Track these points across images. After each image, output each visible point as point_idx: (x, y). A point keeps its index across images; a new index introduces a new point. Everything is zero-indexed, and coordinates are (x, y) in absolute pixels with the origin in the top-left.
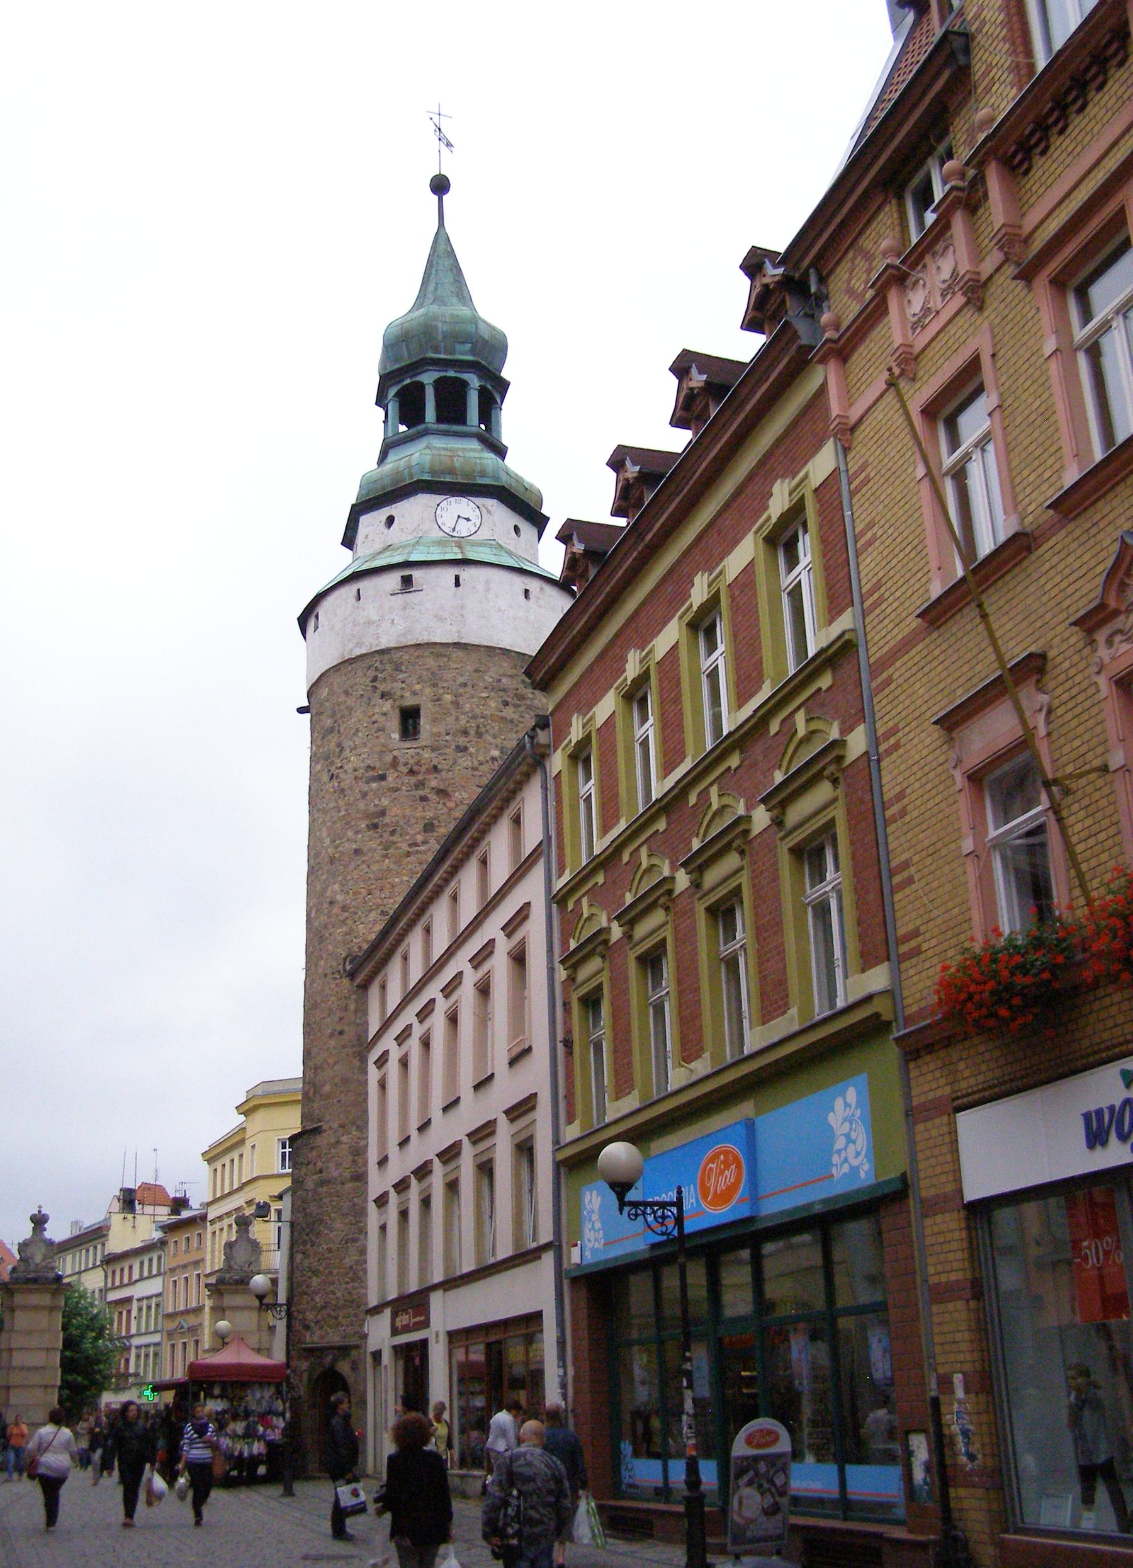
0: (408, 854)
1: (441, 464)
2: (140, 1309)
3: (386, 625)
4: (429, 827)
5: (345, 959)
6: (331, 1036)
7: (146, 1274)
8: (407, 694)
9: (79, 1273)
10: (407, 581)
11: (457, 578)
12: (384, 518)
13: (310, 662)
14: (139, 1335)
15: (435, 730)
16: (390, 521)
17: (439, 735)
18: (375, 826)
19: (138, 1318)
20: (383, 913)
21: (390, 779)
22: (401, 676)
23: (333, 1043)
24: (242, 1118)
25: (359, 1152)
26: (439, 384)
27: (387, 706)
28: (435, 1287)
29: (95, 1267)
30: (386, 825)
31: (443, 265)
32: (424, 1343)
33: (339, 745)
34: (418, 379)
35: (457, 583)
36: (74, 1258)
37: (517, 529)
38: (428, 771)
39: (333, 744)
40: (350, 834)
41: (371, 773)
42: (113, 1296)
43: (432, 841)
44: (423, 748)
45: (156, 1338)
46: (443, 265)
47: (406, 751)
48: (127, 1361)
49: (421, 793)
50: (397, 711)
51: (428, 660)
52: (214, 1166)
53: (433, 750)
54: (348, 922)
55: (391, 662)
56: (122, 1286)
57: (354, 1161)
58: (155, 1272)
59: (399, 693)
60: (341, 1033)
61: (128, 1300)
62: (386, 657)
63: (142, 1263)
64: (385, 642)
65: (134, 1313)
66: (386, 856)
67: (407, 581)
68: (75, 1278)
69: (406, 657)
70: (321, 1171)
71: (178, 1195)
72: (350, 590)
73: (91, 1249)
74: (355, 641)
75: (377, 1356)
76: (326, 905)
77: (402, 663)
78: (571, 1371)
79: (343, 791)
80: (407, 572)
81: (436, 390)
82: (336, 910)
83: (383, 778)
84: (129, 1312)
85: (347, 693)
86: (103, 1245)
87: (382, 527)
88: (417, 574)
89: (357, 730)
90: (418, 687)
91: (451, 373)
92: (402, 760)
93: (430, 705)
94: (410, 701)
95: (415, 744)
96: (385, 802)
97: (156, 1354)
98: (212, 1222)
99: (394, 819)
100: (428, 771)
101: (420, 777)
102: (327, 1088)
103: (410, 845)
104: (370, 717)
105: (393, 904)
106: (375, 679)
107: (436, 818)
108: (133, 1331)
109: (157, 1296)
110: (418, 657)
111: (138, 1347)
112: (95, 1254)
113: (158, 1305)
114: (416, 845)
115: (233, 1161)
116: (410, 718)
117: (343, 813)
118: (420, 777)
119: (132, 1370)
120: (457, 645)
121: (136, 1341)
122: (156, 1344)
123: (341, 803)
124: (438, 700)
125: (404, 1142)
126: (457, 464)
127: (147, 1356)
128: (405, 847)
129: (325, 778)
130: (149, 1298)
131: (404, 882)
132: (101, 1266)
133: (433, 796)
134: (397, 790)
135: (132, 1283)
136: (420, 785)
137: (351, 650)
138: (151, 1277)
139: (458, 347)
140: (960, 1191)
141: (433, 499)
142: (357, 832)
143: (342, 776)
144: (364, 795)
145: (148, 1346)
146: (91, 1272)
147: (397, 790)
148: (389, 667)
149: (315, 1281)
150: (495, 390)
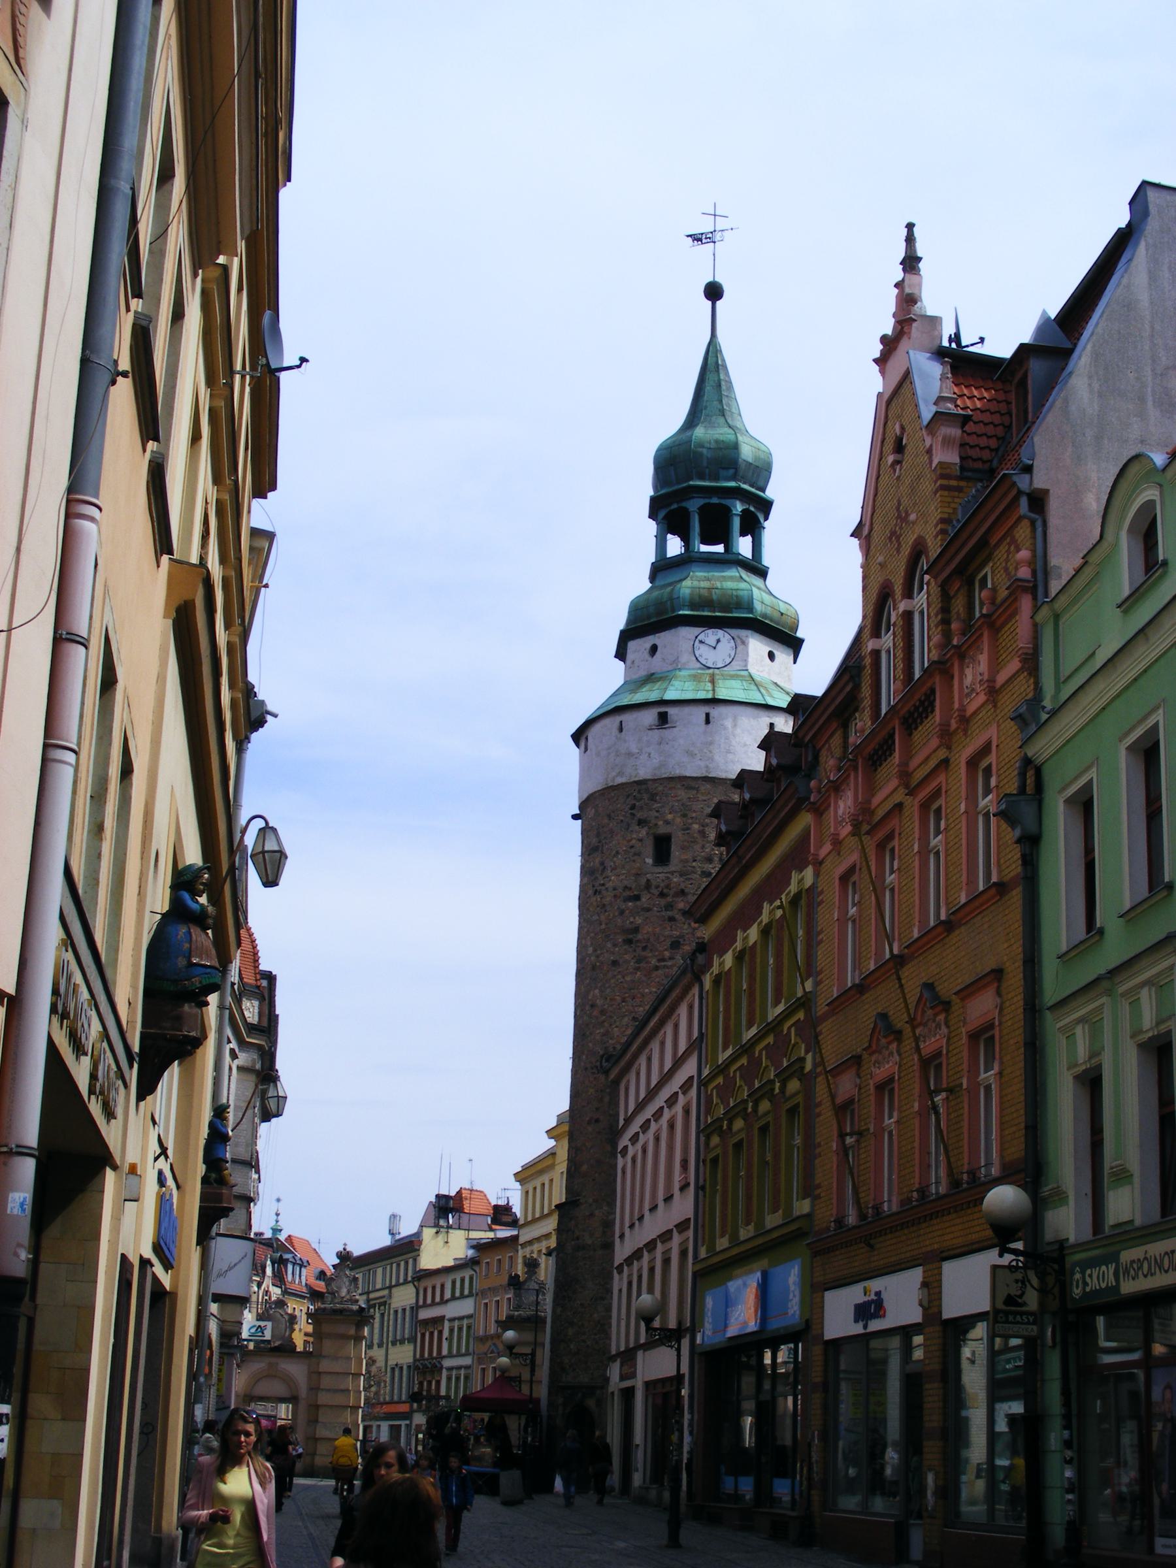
0: (657, 968)
1: (700, 596)
2: (451, 1330)
3: (644, 757)
4: (675, 945)
5: (602, 1056)
6: (589, 1123)
7: (458, 1294)
8: (661, 823)
9: (390, 1287)
10: (663, 719)
11: (707, 715)
12: (648, 645)
13: (585, 772)
14: (450, 1355)
15: (684, 857)
16: (654, 649)
17: (687, 861)
18: (629, 942)
19: (450, 1339)
20: (634, 1019)
21: (644, 900)
22: (656, 805)
23: (590, 1129)
24: (552, 1143)
25: (608, 1225)
26: (703, 510)
27: (643, 832)
28: (639, 1347)
29: (406, 1282)
30: (638, 941)
31: (711, 385)
32: (633, 1387)
33: (602, 863)
34: (684, 504)
35: (708, 721)
36: (384, 1270)
37: (771, 656)
38: (676, 895)
39: (597, 861)
40: (609, 945)
41: (628, 893)
42: (424, 1314)
43: (678, 957)
44: (672, 873)
45: (467, 1361)
46: (711, 385)
47: (658, 875)
48: (438, 1383)
49: (669, 913)
50: (651, 838)
51: (679, 792)
52: (527, 1186)
53: (681, 876)
54: (606, 1024)
55: (647, 790)
56: (433, 1304)
57: (604, 1232)
58: (466, 1292)
59: (653, 821)
60: (597, 1121)
61: (440, 1320)
62: (644, 787)
63: (454, 1282)
64: (644, 773)
65: (446, 1334)
66: (638, 969)
67: (663, 719)
68: (386, 1292)
69: (660, 788)
70: (578, 1238)
71: (500, 1203)
72: (612, 723)
73: (402, 1263)
74: (617, 771)
75: (613, 1393)
76: (587, 1008)
77: (656, 794)
78: (696, 1417)
79: (604, 905)
80: (662, 709)
81: (700, 515)
82: (595, 1013)
83: (637, 898)
84: (441, 1333)
85: (609, 816)
86: (415, 1260)
87: (647, 655)
88: (672, 711)
89: (617, 853)
90: (670, 817)
91: (715, 500)
92: (654, 883)
93: (680, 834)
94: (663, 830)
95: (666, 869)
96: (639, 921)
97: (467, 1378)
98: (524, 1245)
99: (646, 936)
100: (676, 895)
101: (669, 899)
102: (585, 1168)
103: (659, 960)
104: (629, 841)
105: (641, 1011)
106: (633, 807)
107: (682, 936)
108: (445, 1352)
109: (470, 1317)
110: (670, 789)
111: (450, 1369)
112: (406, 1269)
113: (469, 1327)
114: (663, 960)
115: (535, 1189)
116: (662, 848)
117: (603, 926)
118: (669, 899)
119: (443, 1392)
120: (706, 779)
121: (447, 1363)
122: (467, 1367)
123: (603, 917)
124: (688, 829)
125: (632, 1226)
126: (715, 597)
127: (458, 1378)
128: (654, 962)
129: (591, 892)
130: (461, 1318)
131: (651, 991)
132: (413, 1281)
133: (678, 917)
134: (648, 910)
135: (443, 1302)
136: (669, 907)
137: (613, 779)
138: (462, 1296)
139: (723, 473)
140: (940, 1312)
141: (694, 631)
142: (615, 945)
143: (604, 892)
144: (622, 912)
145: (459, 1368)
146: (402, 1288)
147: (648, 910)
148: (646, 796)
149: (570, 1332)
150: (756, 513)
